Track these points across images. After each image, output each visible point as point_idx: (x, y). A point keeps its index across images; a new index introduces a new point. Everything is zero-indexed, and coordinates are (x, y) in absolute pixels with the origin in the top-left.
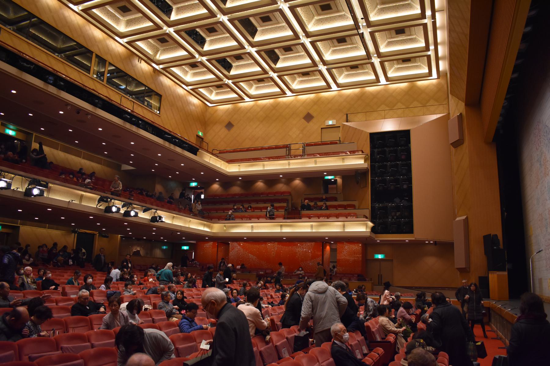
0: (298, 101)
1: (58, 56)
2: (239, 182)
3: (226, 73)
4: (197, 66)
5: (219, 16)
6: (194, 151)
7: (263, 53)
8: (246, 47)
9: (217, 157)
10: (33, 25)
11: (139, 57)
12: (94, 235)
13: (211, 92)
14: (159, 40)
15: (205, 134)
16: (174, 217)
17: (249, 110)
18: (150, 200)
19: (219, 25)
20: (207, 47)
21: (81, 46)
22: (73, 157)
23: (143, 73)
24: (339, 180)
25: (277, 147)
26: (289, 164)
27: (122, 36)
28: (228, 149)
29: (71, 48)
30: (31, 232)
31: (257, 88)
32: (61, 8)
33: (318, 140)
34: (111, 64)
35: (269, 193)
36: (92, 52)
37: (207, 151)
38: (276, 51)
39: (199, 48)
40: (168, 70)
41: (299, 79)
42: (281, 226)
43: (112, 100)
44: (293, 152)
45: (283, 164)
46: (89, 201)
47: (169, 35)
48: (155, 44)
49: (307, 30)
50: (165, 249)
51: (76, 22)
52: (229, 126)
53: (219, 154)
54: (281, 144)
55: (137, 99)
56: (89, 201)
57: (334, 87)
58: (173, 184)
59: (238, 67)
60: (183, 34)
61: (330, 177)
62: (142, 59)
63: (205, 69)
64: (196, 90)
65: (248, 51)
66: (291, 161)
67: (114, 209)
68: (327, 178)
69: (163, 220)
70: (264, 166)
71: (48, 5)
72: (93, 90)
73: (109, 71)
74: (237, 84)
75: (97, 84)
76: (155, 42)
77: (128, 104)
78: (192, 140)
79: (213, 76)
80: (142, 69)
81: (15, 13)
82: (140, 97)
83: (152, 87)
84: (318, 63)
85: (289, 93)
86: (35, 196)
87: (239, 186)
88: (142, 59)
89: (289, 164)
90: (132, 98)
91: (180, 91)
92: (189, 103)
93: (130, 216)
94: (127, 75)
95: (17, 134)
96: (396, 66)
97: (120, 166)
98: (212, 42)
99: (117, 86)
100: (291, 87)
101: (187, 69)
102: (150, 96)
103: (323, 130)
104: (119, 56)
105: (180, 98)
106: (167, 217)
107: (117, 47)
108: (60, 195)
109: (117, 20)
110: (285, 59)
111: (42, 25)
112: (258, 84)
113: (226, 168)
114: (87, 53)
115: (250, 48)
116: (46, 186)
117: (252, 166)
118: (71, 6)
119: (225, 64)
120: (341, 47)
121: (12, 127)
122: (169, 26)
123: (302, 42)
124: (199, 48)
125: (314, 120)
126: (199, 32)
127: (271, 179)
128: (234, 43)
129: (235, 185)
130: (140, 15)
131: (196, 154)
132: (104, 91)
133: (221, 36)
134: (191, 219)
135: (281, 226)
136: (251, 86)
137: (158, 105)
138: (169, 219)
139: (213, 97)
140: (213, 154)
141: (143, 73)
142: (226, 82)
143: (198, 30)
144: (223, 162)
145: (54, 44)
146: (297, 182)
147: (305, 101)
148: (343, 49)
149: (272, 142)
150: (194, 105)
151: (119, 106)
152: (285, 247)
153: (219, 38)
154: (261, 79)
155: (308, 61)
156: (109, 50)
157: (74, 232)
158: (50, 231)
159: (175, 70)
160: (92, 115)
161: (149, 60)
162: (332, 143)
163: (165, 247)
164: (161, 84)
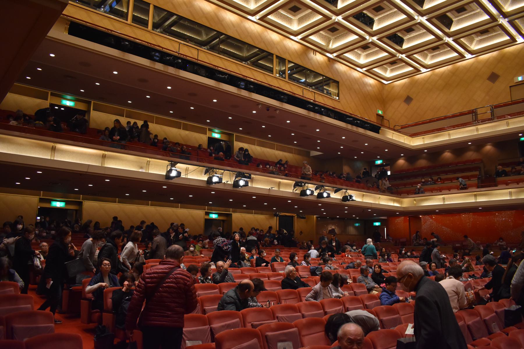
0: (479, 62)
2: (424, 155)
3: (398, 48)
6: (376, 129)
7: (434, 20)
8: (416, 17)
9: (400, 132)
10: (222, 42)
11: (314, 50)
12: (293, 217)
14: (330, 30)
15: (384, 112)
16: (363, 195)
17: (427, 80)
18: (340, 181)
20: (376, 27)
23: (319, 64)
25: (462, 114)
26: (477, 130)
27: (296, 34)
28: (410, 123)
30: (241, 218)
32: (242, 22)
33: (508, 99)
34: (290, 62)
36: (272, 55)
37: (389, 128)
38: (449, 14)
39: (369, 30)
40: (342, 56)
41: (477, 39)
42: (476, 196)
44: (480, 117)
46: (286, 187)
47: (338, 23)
48: (326, 35)
49: (504, 11)
50: (358, 226)
51: (255, 31)
52: (408, 100)
54: (465, 110)
55: (317, 89)
56: (286, 187)
59: (410, 40)
60: (351, 19)
62: (316, 51)
63: (377, 49)
65: (419, 21)
66: (479, 127)
67: (308, 192)
69: (354, 198)
70: (449, 135)
71: (231, 22)
74: (411, 57)
76: (326, 32)
77: (309, 95)
78: (373, 120)
79: (385, 54)
80: (317, 61)
81: (207, 35)
82: (318, 86)
83: (329, 75)
84: (497, 17)
85: (468, 56)
88: (316, 51)
89: (477, 130)
91: (356, 74)
92: (365, 84)
94: (305, 68)
97: (310, 152)
98: (381, 20)
99: (298, 81)
100: (469, 49)
101: (359, 52)
102: (328, 85)
103: (512, 88)
105: (356, 81)
106: (357, 196)
107: (293, 45)
109: (289, 20)
111: (229, 40)
112: (433, 53)
114: (268, 56)
116: (249, 177)
119: (396, 39)
121: (216, 131)
122: (337, 15)
124: (369, 30)
125: (500, 79)
126: (366, 14)
127: (458, 148)
130: (310, 11)
131: (378, 133)
133: (388, 13)
134: (380, 196)
135: (476, 196)
136: (425, 57)
137: (336, 92)
138: (359, 198)
139: (388, 74)
140: (394, 130)
142: (400, 57)
143: (365, 12)
144: (406, 137)
146: (488, 148)
149: (456, 110)
150: (370, 85)
152: (481, 217)
153: (387, 15)
154: (436, 47)
155: (486, 17)
156: (286, 50)
157: (276, 215)
158: (256, 216)
159: (348, 55)
161: (323, 50)
163: (357, 225)
164: (337, 71)
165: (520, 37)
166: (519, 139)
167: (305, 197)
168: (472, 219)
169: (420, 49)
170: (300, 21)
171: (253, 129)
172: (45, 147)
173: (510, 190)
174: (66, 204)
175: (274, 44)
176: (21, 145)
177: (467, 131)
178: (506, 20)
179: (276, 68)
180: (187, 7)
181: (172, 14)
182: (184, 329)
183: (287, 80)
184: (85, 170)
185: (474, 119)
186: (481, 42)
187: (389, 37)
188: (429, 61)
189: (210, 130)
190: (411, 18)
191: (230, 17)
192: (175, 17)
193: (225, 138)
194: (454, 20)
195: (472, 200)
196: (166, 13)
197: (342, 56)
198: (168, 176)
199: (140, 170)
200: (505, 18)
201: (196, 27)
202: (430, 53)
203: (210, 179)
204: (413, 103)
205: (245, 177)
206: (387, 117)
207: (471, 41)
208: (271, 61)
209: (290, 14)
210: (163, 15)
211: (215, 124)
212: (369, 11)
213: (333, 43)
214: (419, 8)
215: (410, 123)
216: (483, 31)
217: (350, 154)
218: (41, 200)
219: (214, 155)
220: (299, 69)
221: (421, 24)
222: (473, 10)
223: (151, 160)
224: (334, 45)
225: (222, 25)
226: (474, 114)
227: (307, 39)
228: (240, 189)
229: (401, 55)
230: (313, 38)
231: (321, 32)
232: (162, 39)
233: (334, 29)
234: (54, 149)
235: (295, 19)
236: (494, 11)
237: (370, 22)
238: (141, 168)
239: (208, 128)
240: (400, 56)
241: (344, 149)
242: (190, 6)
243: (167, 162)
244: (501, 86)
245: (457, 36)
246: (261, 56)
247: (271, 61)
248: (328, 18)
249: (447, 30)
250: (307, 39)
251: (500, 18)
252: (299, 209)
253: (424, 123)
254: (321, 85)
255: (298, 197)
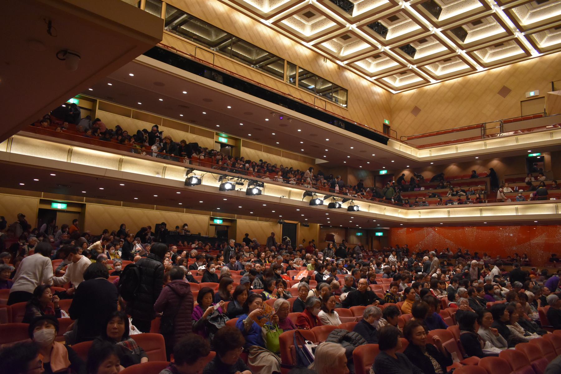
0: (490, 75)
1: (253, 67)
2: (430, 167)
3: (409, 58)
4: (380, 56)
5: (400, 4)
6: (384, 141)
7: (449, 32)
8: (431, 29)
9: (407, 144)
10: (233, 44)
11: (325, 57)
12: (296, 225)
13: (395, 79)
14: (342, 37)
15: (391, 122)
16: (370, 206)
17: (435, 92)
18: (345, 191)
19: (401, 12)
20: (390, 36)
21: (273, 55)
22: (274, 156)
23: (329, 71)
24: (547, 157)
25: (470, 128)
26: (485, 145)
27: (308, 40)
28: (416, 134)
29: (264, 59)
30: (245, 224)
31: (444, 68)
32: (254, 25)
33: (517, 115)
34: (300, 68)
35: (464, 176)
36: (283, 60)
37: (397, 140)
38: (464, 27)
39: (381, 39)
40: (352, 64)
41: (490, 52)
42: (481, 210)
43: (305, 102)
44: (488, 132)
45: (479, 145)
46: (295, 195)
47: (352, 32)
48: (338, 42)
49: (521, 24)
50: (360, 236)
51: (268, 35)
52: (416, 110)
53: (408, 140)
54: (474, 123)
55: (324, 96)
56: (295, 195)
57: (534, 53)
58: (363, 174)
60: (366, 28)
61: (535, 155)
62: (327, 58)
63: (388, 58)
64: (380, 80)
65: (433, 33)
66: (488, 142)
67: (318, 202)
68: (531, 155)
69: (360, 209)
70: (457, 148)
71: (244, 24)
72: (289, 95)
73: (299, 73)
74: (422, 68)
75: (291, 89)
76: (338, 40)
77: (319, 104)
78: (380, 130)
79: (396, 64)
80: (327, 68)
81: (217, 36)
82: (326, 94)
83: (338, 83)
85: (479, 68)
86: (194, 185)
87: (430, 171)
88: (327, 58)
89: (485, 145)
90: (320, 96)
91: (364, 83)
92: (373, 93)
93: (354, 210)
94: (314, 75)
95: (228, 141)
96: (550, 35)
97: (315, 160)
98: (394, 30)
99: (305, 87)
100: (481, 62)
102: (336, 92)
103: (523, 103)
104: (307, 59)
105: (365, 90)
106: (364, 206)
107: (303, 51)
108: (272, 192)
109: (302, 26)
110: (474, 34)
111: (239, 42)
112: (444, 64)
113: (417, 154)
114: (278, 60)
115: (435, 29)
116: (262, 186)
117: (444, 150)
118: (262, 20)
119: (409, 50)
120: (542, 8)
121: (224, 135)
122: (352, 23)
123: (494, 11)
124: (381, 39)
126: (380, 23)
127: (465, 162)
128: (417, 27)
129: (426, 170)
130: (324, 17)
131: (386, 144)
132: (297, 94)
133: (403, 23)
134: (386, 207)
135: (481, 210)
136: (436, 68)
137: (345, 99)
138: (363, 207)
139: (397, 83)
140: (402, 142)
141: (328, 70)
142: (410, 68)
143: (379, 21)
144: (413, 149)
145: (207, 38)
146: (495, 163)
147: (499, 75)
148: (545, 9)
149: (464, 123)
150: (378, 94)
151: (193, 59)
153: (401, 25)
154: (448, 58)
155: (502, 30)
156: (298, 56)
157: (281, 223)
158: (261, 222)
159: (360, 64)
160: (292, 119)
161: (334, 58)
162: (536, 117)
163: (359, 234)
164: (346, 80)
165: (535, 51)
166: (527, 155)
167: (251, 197)
168: (475, 233)
169: (434, 60)
170: (314, 26)
171: (262, 137)
172: (62, 150)
173: (517, 206)
174: (68, 206)
175: (285, 48)
176: (440, 212)
177: (475, 146)
178: (523, 34)
179: (288, 73)
180: (200, 7)
181: (182, 13)
182: (7, 300)
183: (297, 86)
184: (102, 174)
185: (483, 133)
186: (494, 54)
187: (402, 48)
188: (439, 72)
189: (217, 134)
190: (426, 29)
191: (242, 19)
192: (185, 16)
193: (232, 143)
194: (469, 32)
195: (477, 214)
196: (176, 11)
197: (352, 64)
198: (188, 182)
199: (157, 176)
200: (521, 32)
201: (206, 27)
202: (441, 64)
203: (223, 185)
204: (421, 113)
205: (259, 186)
206: (393, 127)
207: (484, 54)
208: (282, 67)
209: (303, 18)
210: (173, 12)
211: (223, 129)
212: (384, 21)
213: (344, 50)
214: (434, 19)
215: (416, 134)
216: (497, 44)
217: (354, 165)
218: (42, 202)
219: (224, 161)
220: (308, 75)
221: (435, 36)
222: (490, 23)
223: (167, 165)
224: (346, 52)
225: (234, 27)
226: (483, 128)
227: (319, 46)
228: (192, 188)
229: (411, 65)
230: (326, 45)
231: (334, 39)
232: (175, 39)
233: (347, 37)
234: (70, 152)
235: (308, 24)
236: (511, 25)
237: (383, 31)
238: (158, 173)
239: (215, 132)
240: (410, 66)
241: (350, 157)
242: (203, 6)
243: (183, 168)
244: (512, 100)
245: (470, 49)
246: (271, 61)
247: (282, 67)
248: (342, 26)
249: (460, 42)
250: (319, 46)
251: (516, 31)
252: (305, 217)
253: (430, 135)
254: (330, 91)
255: (307, 206)
